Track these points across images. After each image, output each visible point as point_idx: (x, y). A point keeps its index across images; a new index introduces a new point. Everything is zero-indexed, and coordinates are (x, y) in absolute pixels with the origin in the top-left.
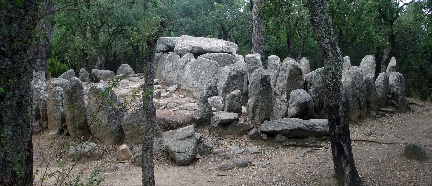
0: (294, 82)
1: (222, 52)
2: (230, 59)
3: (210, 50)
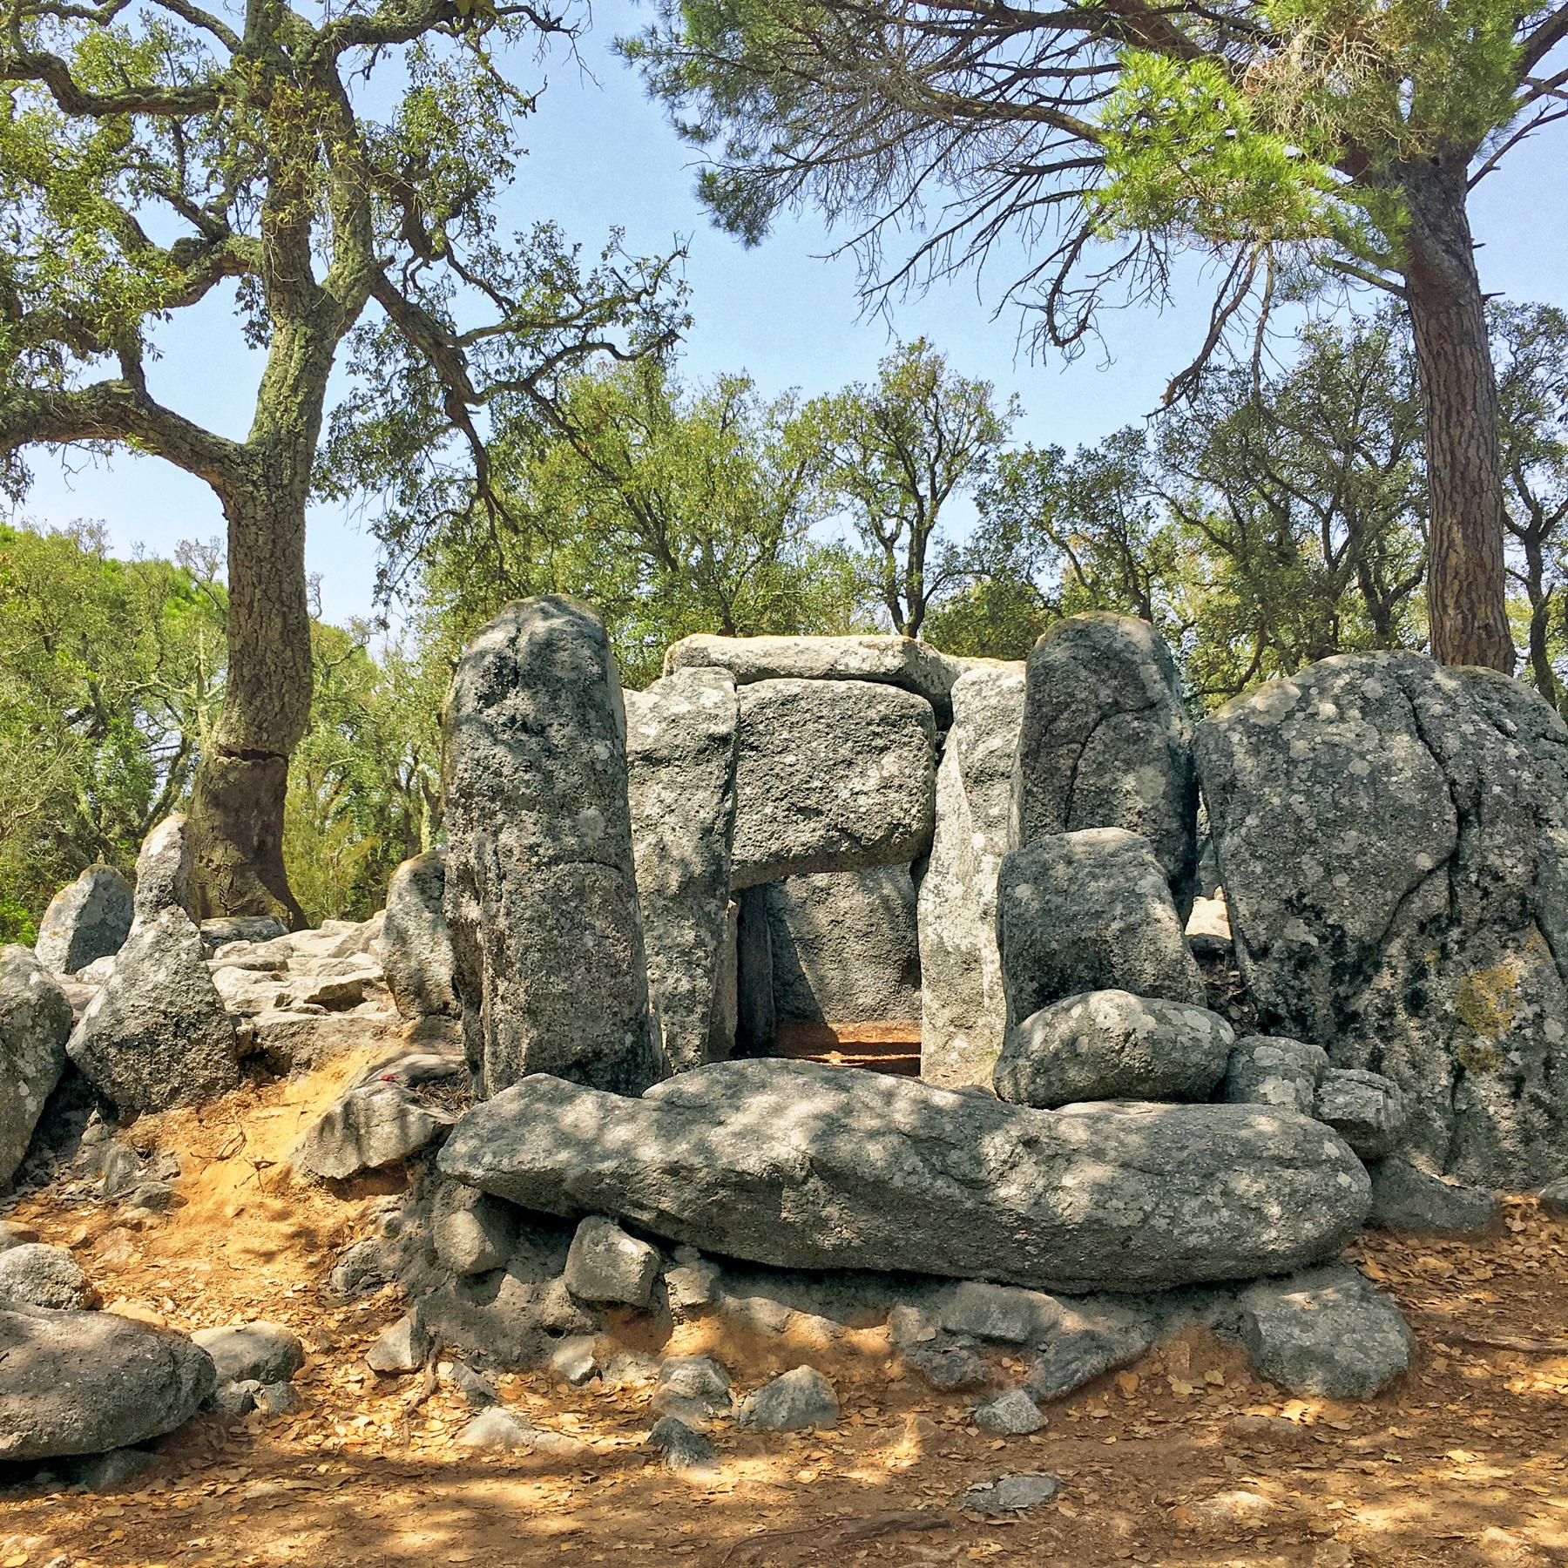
0: (1078, 782)
1: (831, 674)
2: (884, 720)
3: (753, 660)
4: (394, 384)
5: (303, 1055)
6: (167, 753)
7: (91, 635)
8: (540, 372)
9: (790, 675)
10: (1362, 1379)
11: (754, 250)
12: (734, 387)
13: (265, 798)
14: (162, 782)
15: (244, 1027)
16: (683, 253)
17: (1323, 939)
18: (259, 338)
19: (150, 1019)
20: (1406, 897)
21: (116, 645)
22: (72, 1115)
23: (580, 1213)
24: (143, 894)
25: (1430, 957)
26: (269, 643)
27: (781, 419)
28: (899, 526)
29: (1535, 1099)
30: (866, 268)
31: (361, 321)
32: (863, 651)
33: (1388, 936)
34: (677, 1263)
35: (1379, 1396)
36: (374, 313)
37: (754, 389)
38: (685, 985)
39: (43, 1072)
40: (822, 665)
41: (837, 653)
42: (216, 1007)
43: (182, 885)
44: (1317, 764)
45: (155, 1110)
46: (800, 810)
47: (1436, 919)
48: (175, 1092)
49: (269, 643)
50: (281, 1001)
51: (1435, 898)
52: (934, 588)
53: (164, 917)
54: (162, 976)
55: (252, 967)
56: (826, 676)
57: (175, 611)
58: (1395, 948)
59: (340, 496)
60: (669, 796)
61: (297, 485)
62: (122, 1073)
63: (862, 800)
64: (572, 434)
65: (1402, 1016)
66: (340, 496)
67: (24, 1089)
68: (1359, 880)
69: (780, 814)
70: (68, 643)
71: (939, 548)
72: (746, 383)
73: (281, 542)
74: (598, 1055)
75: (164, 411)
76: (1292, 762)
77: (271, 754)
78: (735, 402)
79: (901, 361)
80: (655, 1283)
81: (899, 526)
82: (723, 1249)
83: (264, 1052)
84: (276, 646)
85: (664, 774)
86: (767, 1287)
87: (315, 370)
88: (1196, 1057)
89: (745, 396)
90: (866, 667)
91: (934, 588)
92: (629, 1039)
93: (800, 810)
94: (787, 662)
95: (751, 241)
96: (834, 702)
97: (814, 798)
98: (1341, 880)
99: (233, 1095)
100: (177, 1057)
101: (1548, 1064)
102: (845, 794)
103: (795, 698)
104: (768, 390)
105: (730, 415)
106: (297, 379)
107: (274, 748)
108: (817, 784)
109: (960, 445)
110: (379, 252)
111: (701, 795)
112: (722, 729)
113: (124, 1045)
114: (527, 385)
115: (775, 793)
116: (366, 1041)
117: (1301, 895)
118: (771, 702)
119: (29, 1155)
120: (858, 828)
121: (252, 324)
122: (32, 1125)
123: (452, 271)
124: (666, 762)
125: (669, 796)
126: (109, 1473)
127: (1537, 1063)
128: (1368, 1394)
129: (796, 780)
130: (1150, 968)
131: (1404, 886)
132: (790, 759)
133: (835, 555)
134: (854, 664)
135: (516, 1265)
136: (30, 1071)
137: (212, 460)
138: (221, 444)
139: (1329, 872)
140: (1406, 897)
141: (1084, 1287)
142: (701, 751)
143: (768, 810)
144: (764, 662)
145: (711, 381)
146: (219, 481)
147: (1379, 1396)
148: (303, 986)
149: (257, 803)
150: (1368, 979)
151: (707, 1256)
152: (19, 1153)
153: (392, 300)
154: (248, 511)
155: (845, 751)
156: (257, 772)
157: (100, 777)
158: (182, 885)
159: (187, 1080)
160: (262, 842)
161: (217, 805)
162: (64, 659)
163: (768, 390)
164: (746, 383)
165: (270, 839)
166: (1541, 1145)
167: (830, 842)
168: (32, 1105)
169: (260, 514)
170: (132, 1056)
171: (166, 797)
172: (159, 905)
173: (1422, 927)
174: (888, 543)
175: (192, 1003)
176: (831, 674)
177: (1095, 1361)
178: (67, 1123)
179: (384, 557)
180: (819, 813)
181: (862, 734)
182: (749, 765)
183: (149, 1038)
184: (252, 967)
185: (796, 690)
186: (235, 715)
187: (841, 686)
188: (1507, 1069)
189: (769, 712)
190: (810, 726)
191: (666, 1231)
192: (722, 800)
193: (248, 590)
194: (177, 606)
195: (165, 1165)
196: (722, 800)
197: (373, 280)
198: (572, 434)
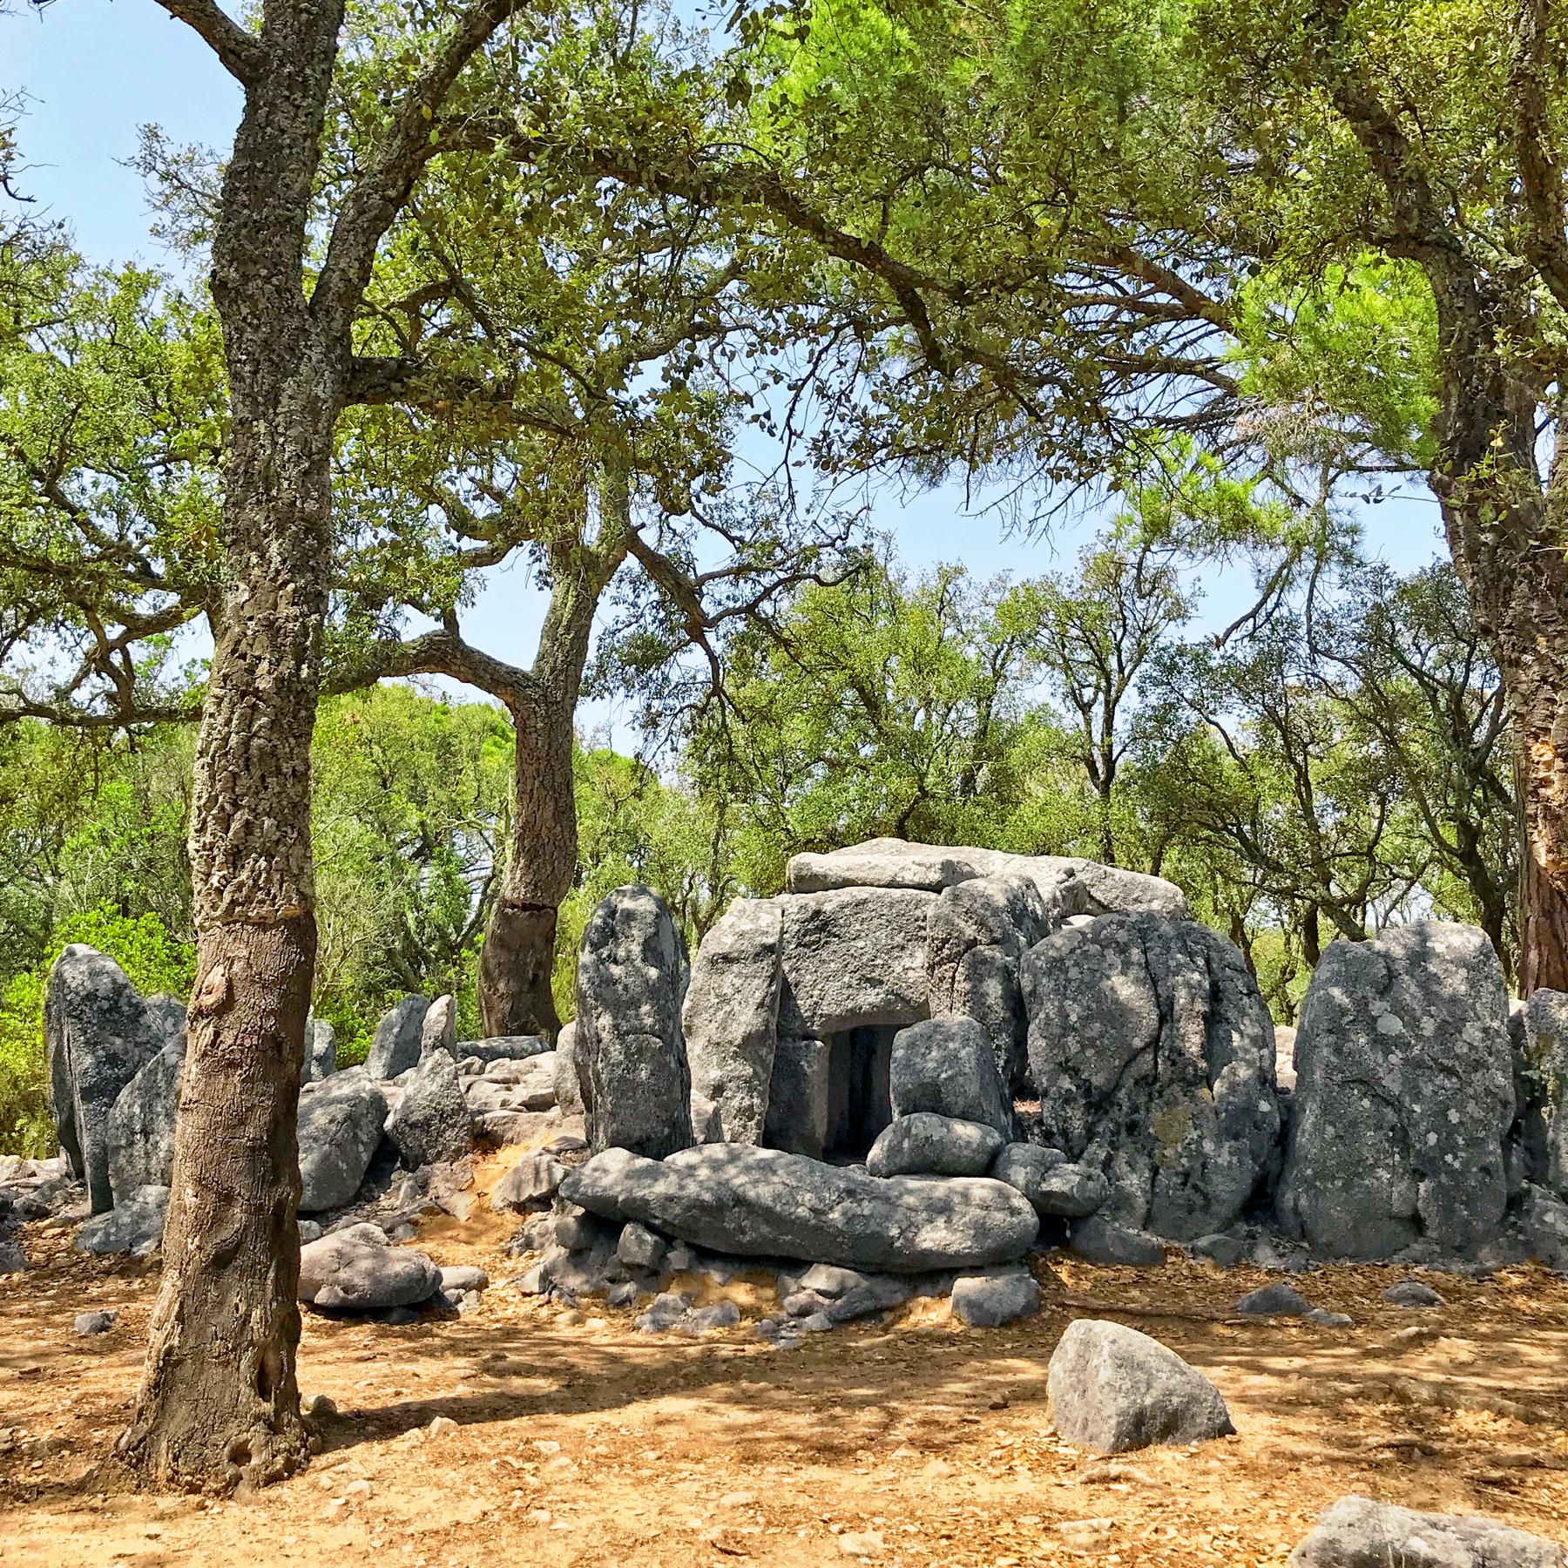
1: (893, 884)
4: (647, 612)
5: (509, 1135)
6: (483, 873)
7: (421, 773)
8: (760, 599)
9: (864, 884)
10: (994, 1316)
11: (935, 490)
12: (949, 575)
13: (538, 941)
14: (476, 899)
15: (479, 1118)
16: (869, 508)
17: (1078, 1087)
18: (546, 583)
19: (427, 1112)
20: (1127, 1064)
21: (443, 784)
22: (387, 1166)
23: (627, 1220)
24: (427, 1041)
25: (1143, 1099)
26: (545, 821)
27: (994, 597)
28: (1096, 694)
29: (1195, 1187)
30: (1008, 521)
31: (623, 566)
32: (915, 868)
33: (1118, 1087)
34: (674, 1249)
35: (1002, 1325)
36: (631, 562)
37: (968, 576)
38: (746, 1102)
39: (371, 1138)
40: (886, 878)
41: (896, 869)
42: (462, 1108)
43: (447, 1036)
44: (1082, 981)
45: (429, 1163)
46: (868, 980)
47: (1145, 1077)
48: (439, 1154)
49: (545, 821)
50: (504, 1104)
51: (1145, 1063)
52: (1124, 750)
53: (437, 1054)
54: (434, 1088)
55: (496, 1082)
56: (888, 886)
57: (493, 749)
58: (1122, 1094)
59: (606, 695)
60: (738, 982)
61: (568, 701)
62: (411, 1141)
63: (911, 973)
64: (787, 644)
65: (1124, 1134)
66: (606, 695)
67: (361, 1148)
68: (1100, 1053)
69: (854, 982)
70: (401, 784)
71: (1125, 716)
72: (960, 571)
73: (554, 744)
74: (649, 1139)
75: (472, 651)
76: (1069, 981)
77: (544, 907)
78: (949, 588)
79: (1100, 548)
80: (662, 1257)
81: (1096, 694)
82: (697, 1242)
83: (488, 1133)
84: (550, 823)
85: (735, 968)
86: (719, 1264)
87: (585, 609)
88: (966, 1152)
89: (962, 582)
90: (916, 879)
91: (1124, 750)
92: (666, 1131)
93: (868, 980)
94: (863, 875)
95: (933, 483)
96: (892, 905)
97: (878, 971)
98: (1090, 1053)
99: (470, 1156)
100: (440, 1134)
101: (1204, 1166)
102: (899, 969)
103: (865, 902)
104: (980, 573)
105: (947, 596)
106: (570, 621)
107: (546, 902)
108: (879, 961)
109: (1148, 622)
110: (635, 520)
111: (757, 981)
112: (770, 940)
113: (413, 1126)
114: (751, 609)
115: (851, 968)
116: (543, 1128)
117: (1067, 1060)
118: (849, 904)
119: (363, 1184)
120: (908, 993)
121: (540, 573)
122: (365, 1168)
123: (695, 520)
124: (737, 960)
125: (738, 982)
126: (395, 1316)
127: (1198, 1166)
128: (997, 1323)
129: (865, 959)
130: (961, 1101)
131: (1126, 1058)
132: (861, 944)
133: (1040, 716)
134: (909, 877)
135: (595, 1248)
136: (365, 1139)
137: (506, 685)
138: (515, 672)
139: (1083, 1048)
140: (1127, 1064)
141: (872, 1268)
142: (757, 955)
143: (846, 979)
144: (847, 875)
145: (932, 570)
146: (510, 700)
147: (1002, 1325)
148: (520, 1094)
149: (533, 945)
150: (1106, 1112)
151: (689, 1245)
152: (358, 1183)
153: (646, 555)
154: (531, 722)
155: (899, 939)
156: (534, 920)
157: (424, 893)
158: (447, 1036)
159: (445, 1148)
160: (536, 976)
161: (502, 946)
162: (399, 801)
163: (980, 573)
164: (960, 571)
165: (541, 973)
166: (1197, 1214)
167: (889, 1002)
168: (365, 1157)
169: (540, 725)
170: (417, 1132)
171: (479, 915)
172: (434, 1047)
173: (1136, 1083)
174: (1085, 708)
175: (449, 1104)
176: (893, 884)
177: (868, 1304)
178: (383, 1169)
179: (640, 743)
180: (881, 982)
181: (911, 927)
182: (834, 947)
183: (425, 1124)
184: (496, 1082)
185: (865, 896)
186: (518, 876)
187: (896, 893)
188: (1180, 1169)
189: (847, 911)
190: (876, 922)
191: (668, 1230)
192: (770, 985)
193: (529, 781)
194: (495, 744)
195: (432, 1193)
196: (770, 985)
197: (631, 542)
198: (787, 644)
